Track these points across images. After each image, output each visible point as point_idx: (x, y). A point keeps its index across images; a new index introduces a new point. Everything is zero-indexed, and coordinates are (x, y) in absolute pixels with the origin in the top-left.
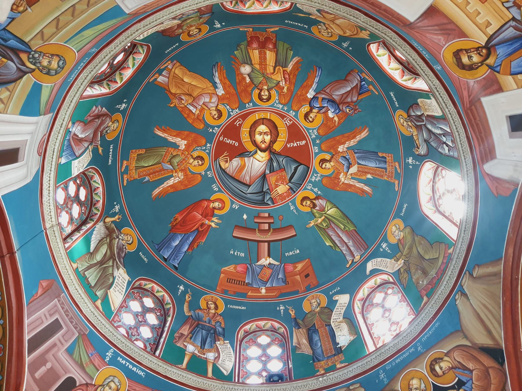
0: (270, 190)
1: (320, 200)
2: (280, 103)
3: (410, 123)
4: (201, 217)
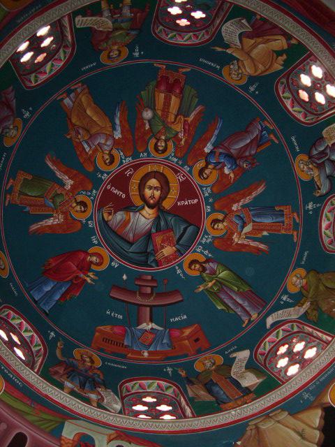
0: (155, 251)
1: (211, 264)
2: (175, 156)
3: (310, 166)
4: (75, 268)
